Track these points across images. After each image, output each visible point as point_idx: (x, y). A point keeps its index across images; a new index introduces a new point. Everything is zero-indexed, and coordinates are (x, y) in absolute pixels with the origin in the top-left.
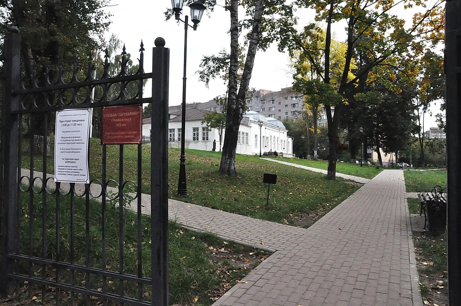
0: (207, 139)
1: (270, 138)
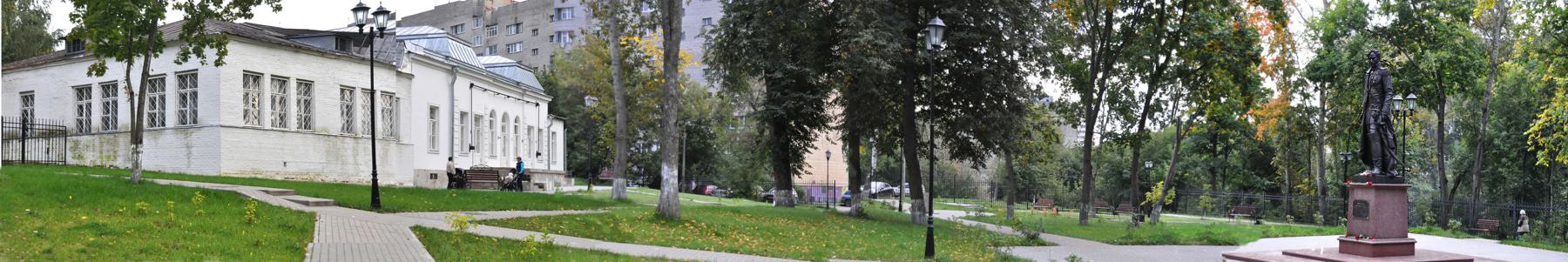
0: (195, 121)
1: (487, 118)
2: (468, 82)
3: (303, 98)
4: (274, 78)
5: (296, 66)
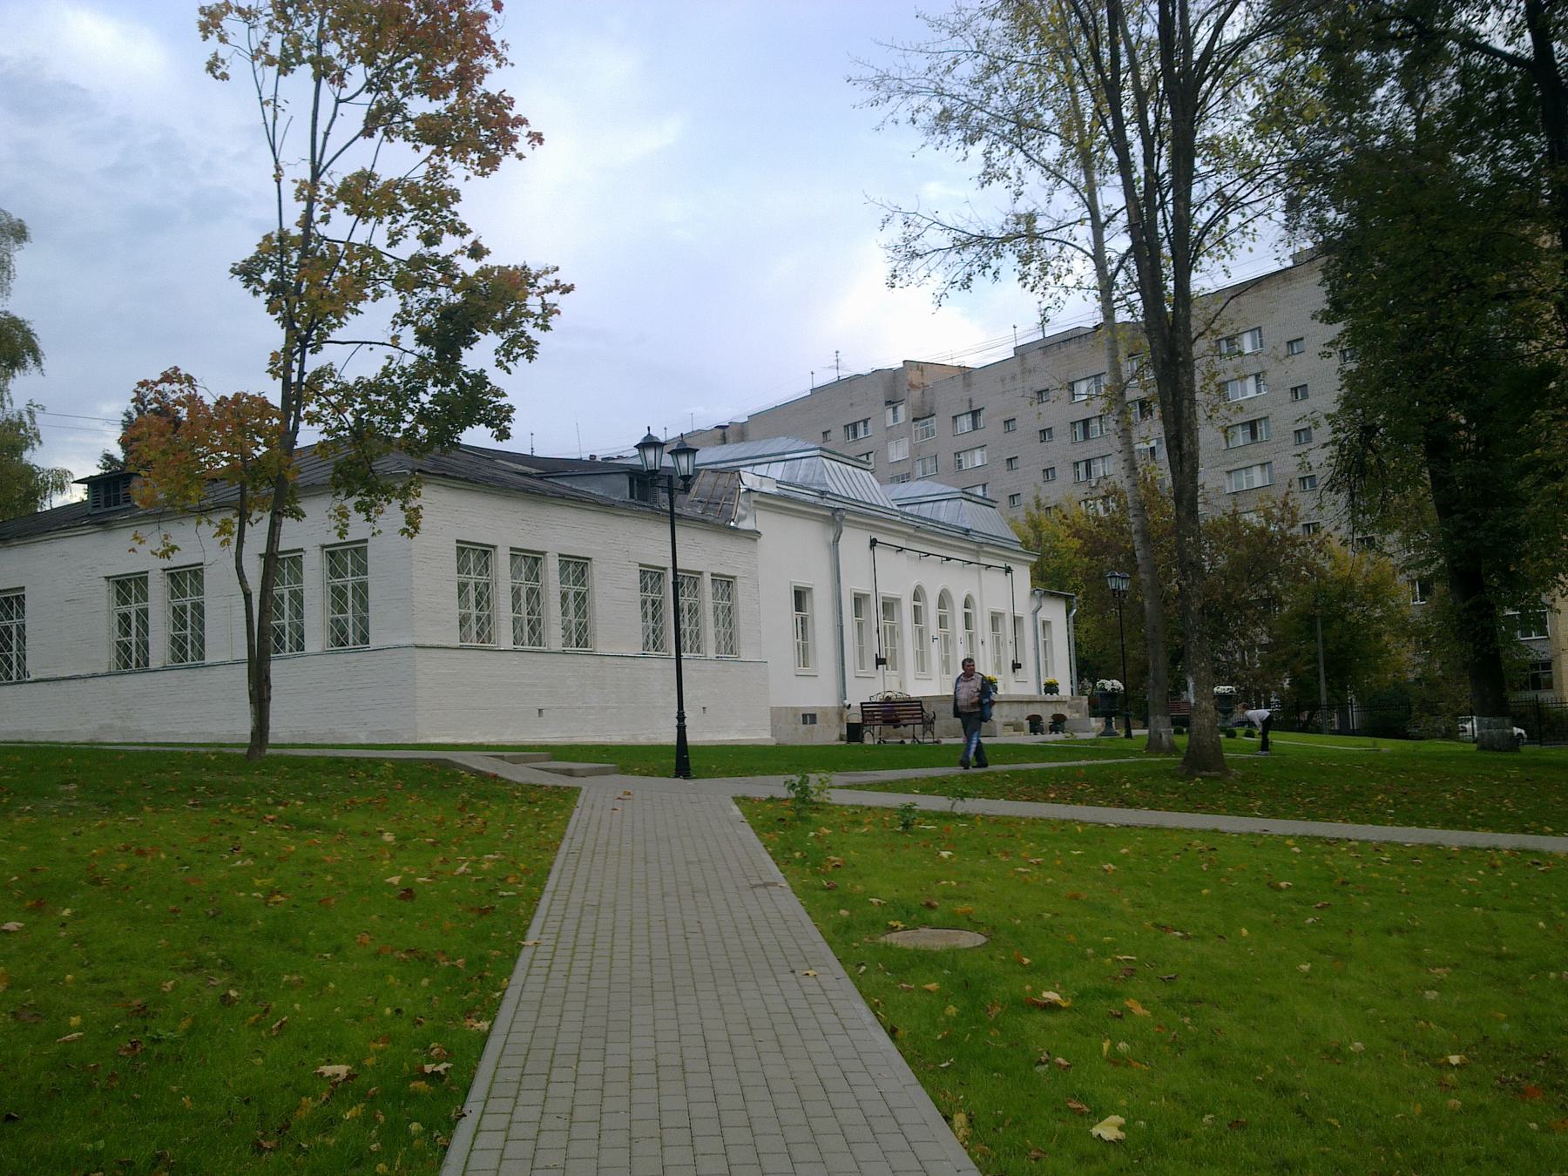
2: (864, 537)
3: (572, 590)
4: (515, 553)
5: (558, 531)
